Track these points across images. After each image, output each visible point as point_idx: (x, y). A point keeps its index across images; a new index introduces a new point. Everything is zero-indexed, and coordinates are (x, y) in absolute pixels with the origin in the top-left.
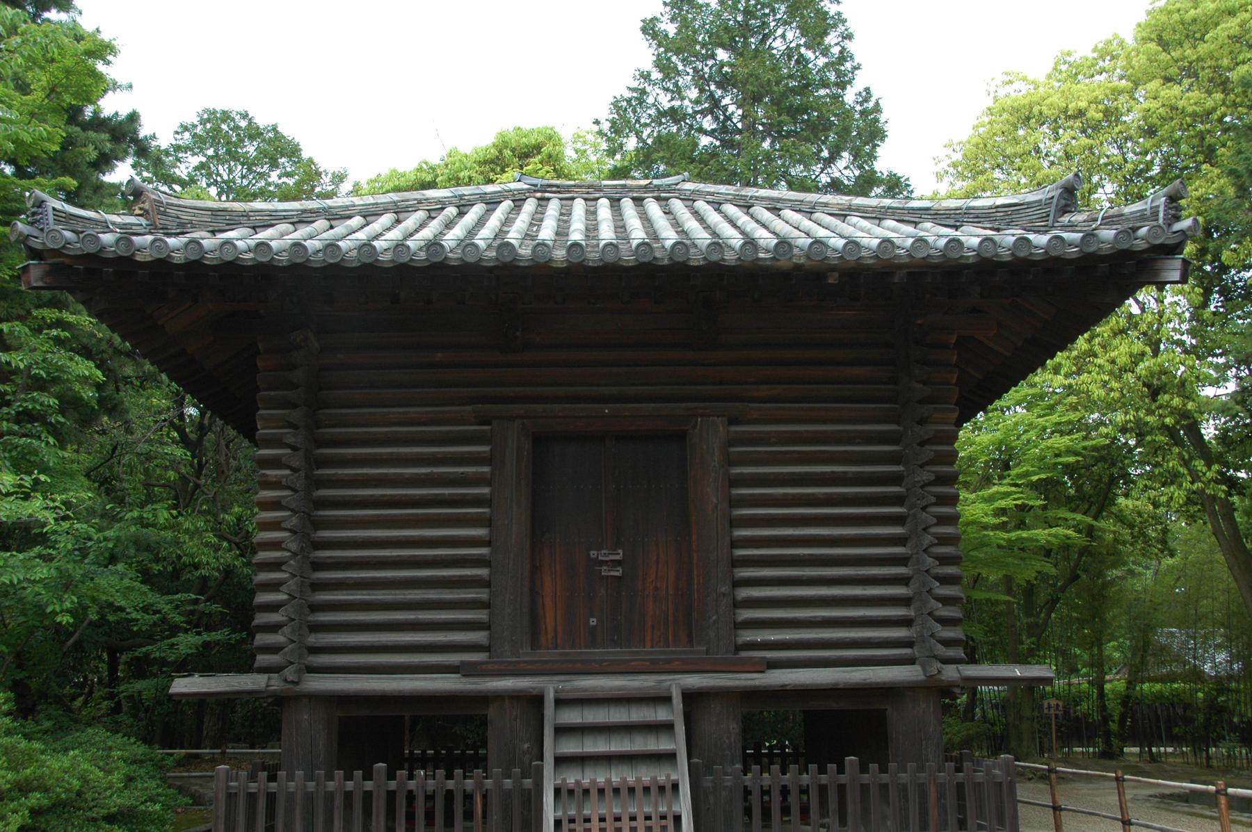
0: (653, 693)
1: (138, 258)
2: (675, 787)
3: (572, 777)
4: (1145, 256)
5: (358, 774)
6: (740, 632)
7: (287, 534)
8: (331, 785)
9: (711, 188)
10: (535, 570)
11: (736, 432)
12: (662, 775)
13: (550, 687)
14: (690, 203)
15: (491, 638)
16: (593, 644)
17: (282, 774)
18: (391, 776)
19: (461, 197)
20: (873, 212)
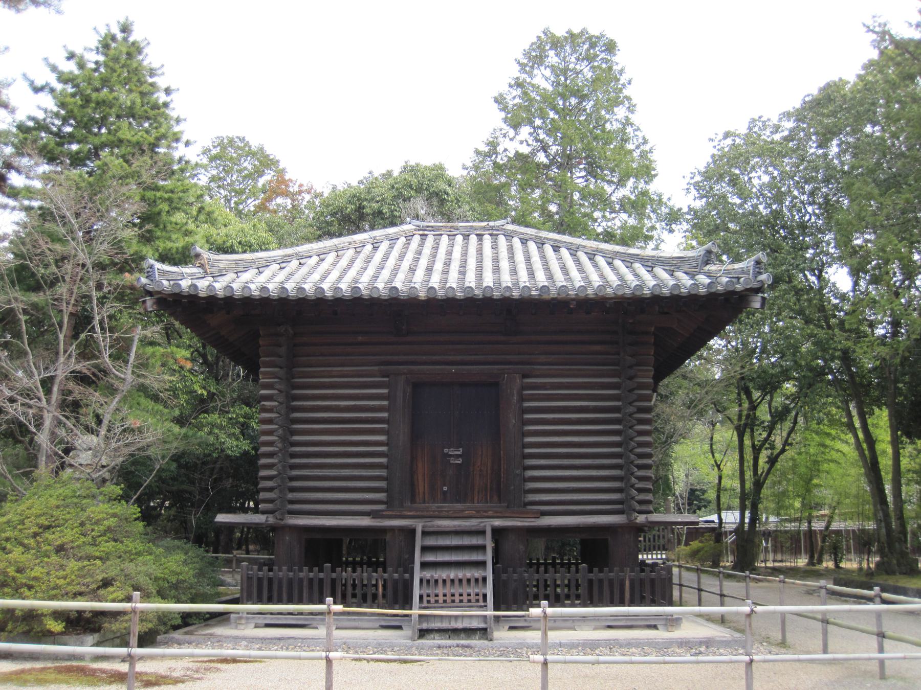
0: (473, 529)
1: (200, 295)
2: (484, 579)
4: (744, 293)
5: (316, 569)
6: (527, 495)
7: (277, 438)
8: (301, 575)
9: (522, 229)
11: (527, 383)
12: (477, 573)
13: (419, 525)
16: (445, 500)
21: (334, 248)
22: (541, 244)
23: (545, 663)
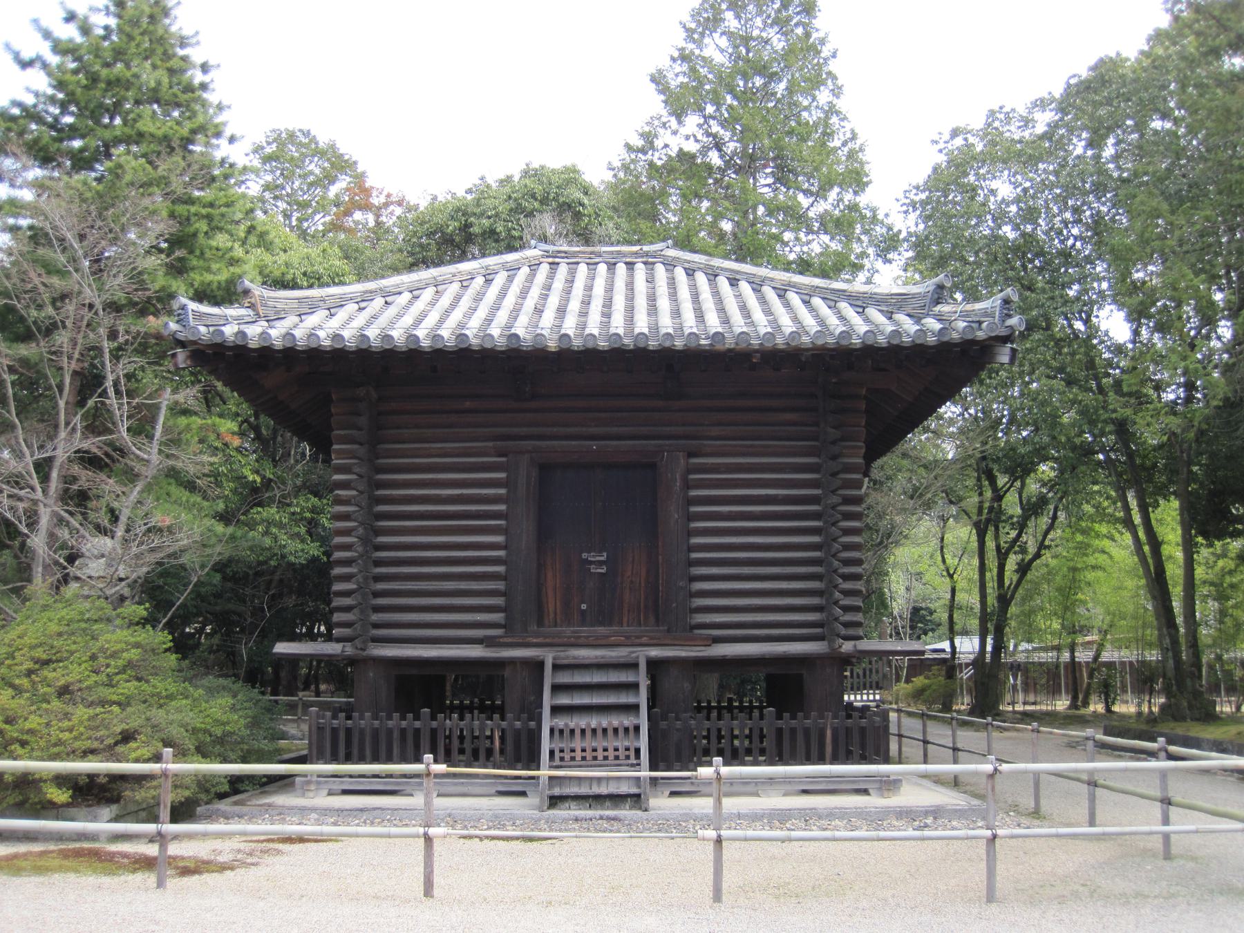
0: (622, 660)
3: (560, 722)
5: (410, 716)
8: (390, 723)
10: (541, 567)
11: (695, 464)
12: (627, 721)
13: (549, 657)
14: (671, 268)
15: (507, 618)
16: (583, 622)
17: (355, 715)
18: (433, 718)
19: (487, 268)
20: (805, 289)
21: (432, 281)
22: (713, 275)
23: (719, 841)
